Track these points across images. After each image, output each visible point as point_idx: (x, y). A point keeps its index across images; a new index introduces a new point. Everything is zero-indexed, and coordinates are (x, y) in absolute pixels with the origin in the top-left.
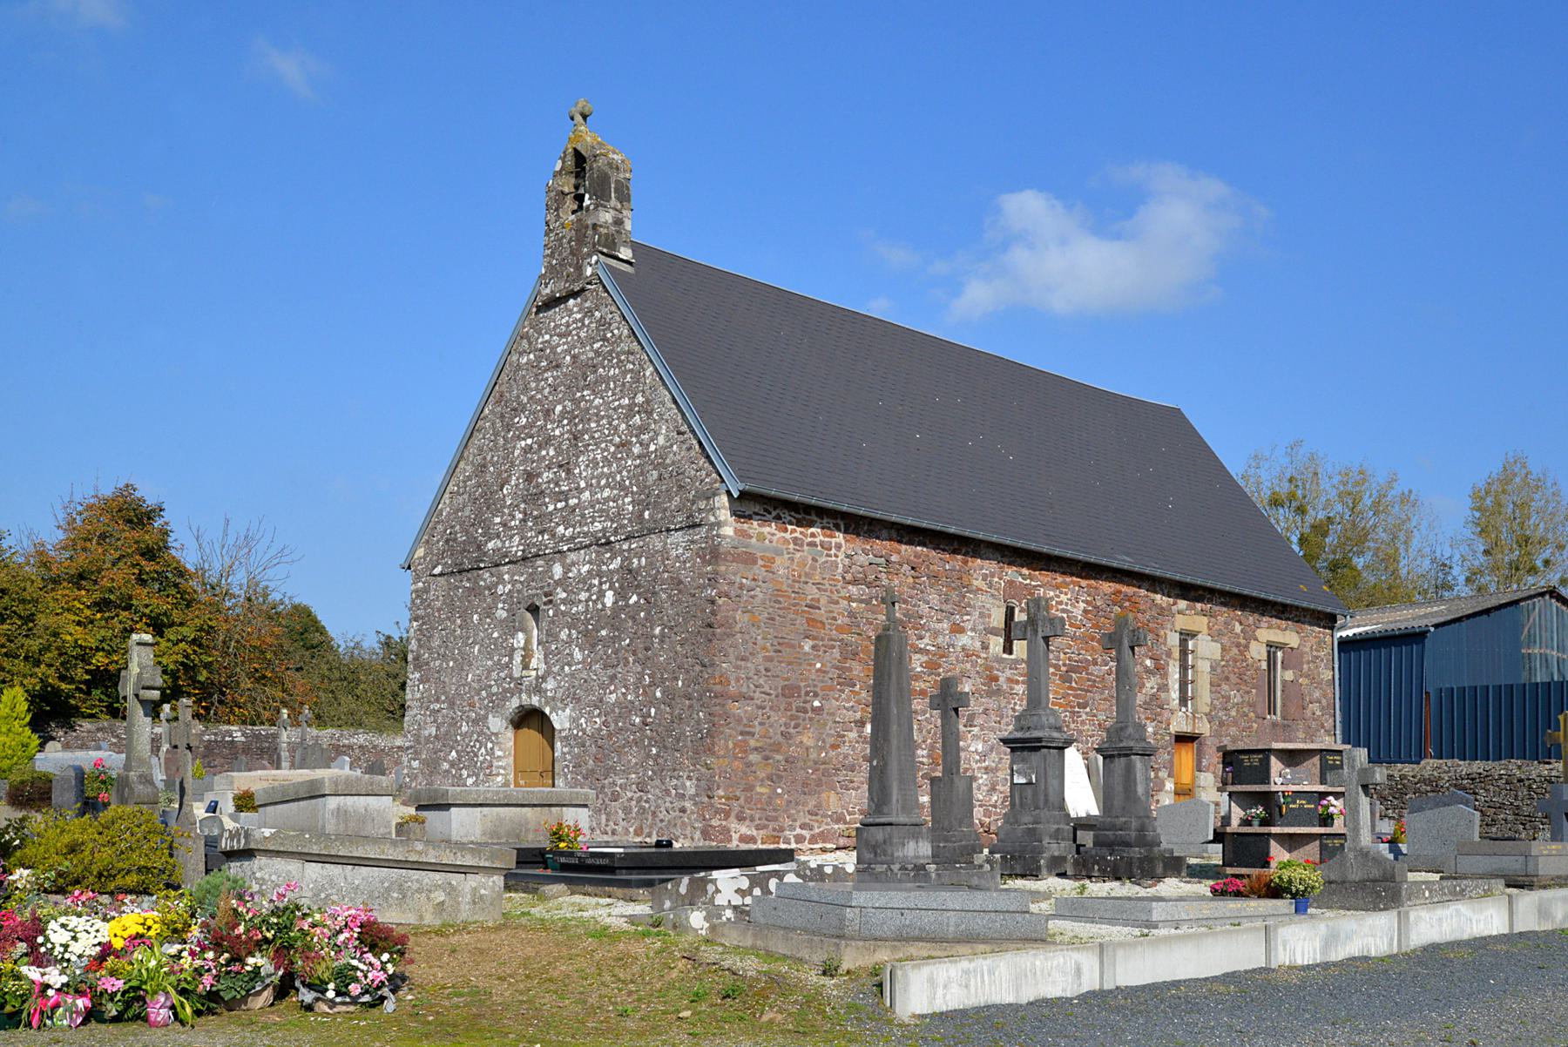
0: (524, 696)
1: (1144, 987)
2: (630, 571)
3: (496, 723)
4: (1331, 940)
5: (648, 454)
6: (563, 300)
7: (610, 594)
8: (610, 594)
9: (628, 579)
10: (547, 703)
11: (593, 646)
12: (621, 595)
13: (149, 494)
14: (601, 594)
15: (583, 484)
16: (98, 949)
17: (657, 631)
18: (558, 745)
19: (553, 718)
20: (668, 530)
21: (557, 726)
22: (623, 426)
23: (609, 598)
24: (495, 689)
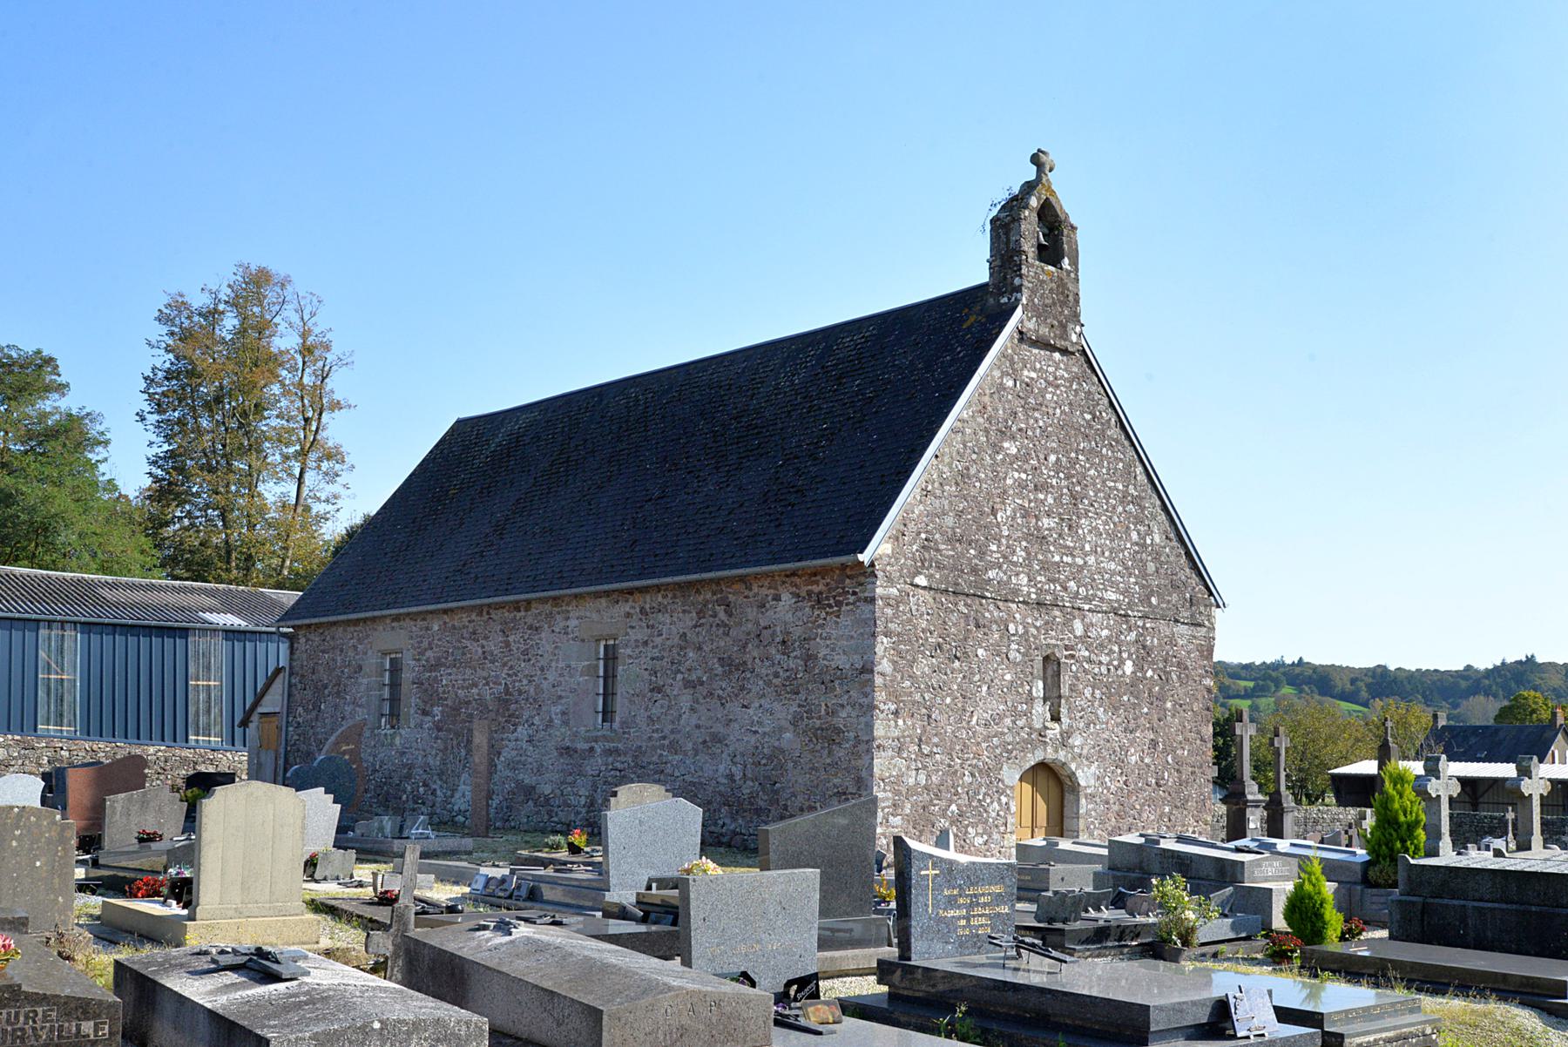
0: (1049, 749)
1: (1492, 950)
2: (1144, 647)
3: (1011, 775)
4: (1313, 995)
5: (1144, 545)
6: (1054, 348)
7: (1129, 664)
8: (1129, 664)
9: (1144, 654)
10: (1074, 759)
11: (1116, 709)
12: (1139, 667)
13: (184, 292)
14: (1122, 662)
15: (1087, 548)
16: (1142, 840)
17: (1169, 705)
18: (1083, 801)
19: (1079, 774)
20: (1177, 621)
21: (1083, 783)
22: (1120, 509)
23: (1129, 667)
24: (1009, 738)
